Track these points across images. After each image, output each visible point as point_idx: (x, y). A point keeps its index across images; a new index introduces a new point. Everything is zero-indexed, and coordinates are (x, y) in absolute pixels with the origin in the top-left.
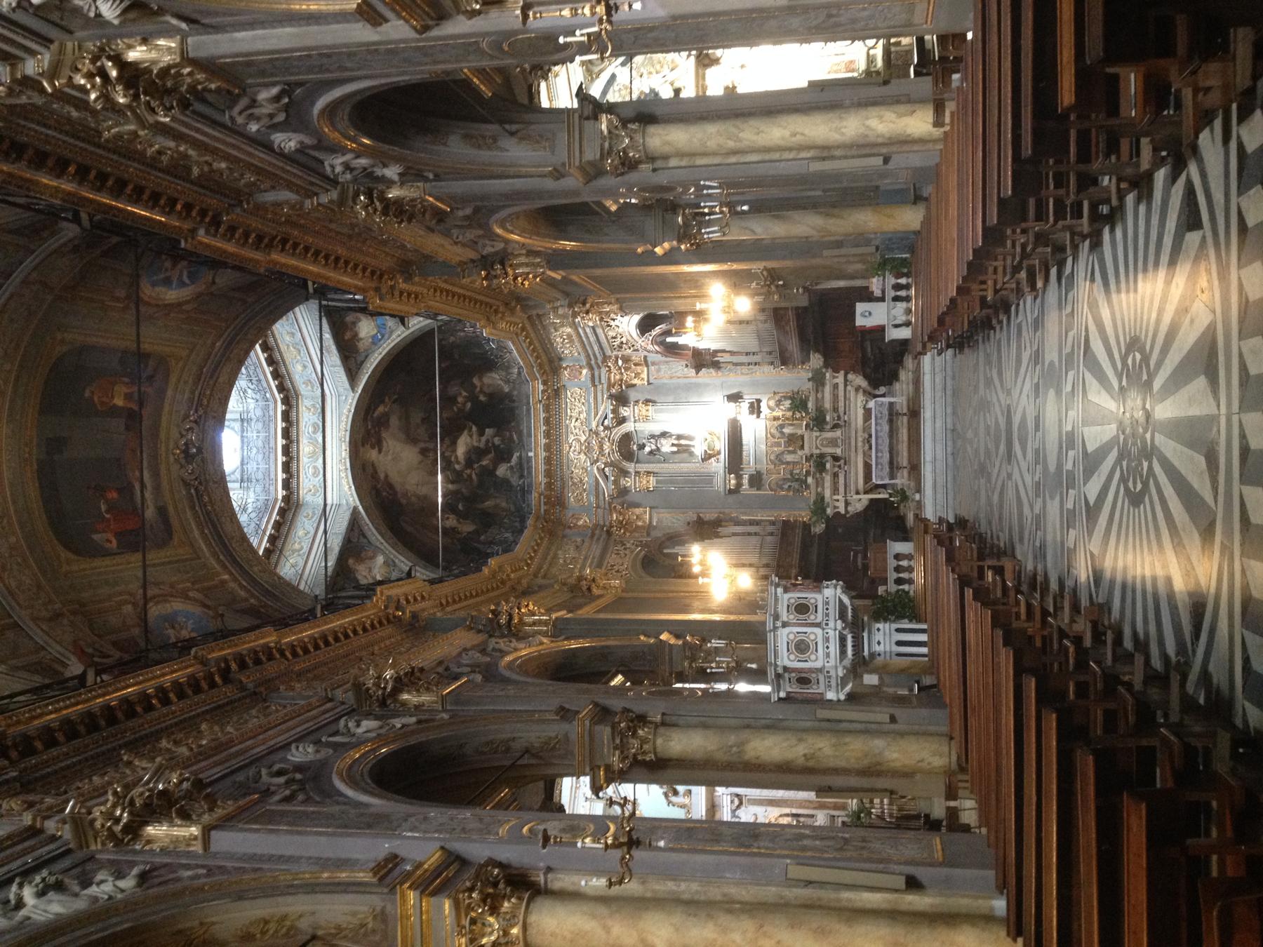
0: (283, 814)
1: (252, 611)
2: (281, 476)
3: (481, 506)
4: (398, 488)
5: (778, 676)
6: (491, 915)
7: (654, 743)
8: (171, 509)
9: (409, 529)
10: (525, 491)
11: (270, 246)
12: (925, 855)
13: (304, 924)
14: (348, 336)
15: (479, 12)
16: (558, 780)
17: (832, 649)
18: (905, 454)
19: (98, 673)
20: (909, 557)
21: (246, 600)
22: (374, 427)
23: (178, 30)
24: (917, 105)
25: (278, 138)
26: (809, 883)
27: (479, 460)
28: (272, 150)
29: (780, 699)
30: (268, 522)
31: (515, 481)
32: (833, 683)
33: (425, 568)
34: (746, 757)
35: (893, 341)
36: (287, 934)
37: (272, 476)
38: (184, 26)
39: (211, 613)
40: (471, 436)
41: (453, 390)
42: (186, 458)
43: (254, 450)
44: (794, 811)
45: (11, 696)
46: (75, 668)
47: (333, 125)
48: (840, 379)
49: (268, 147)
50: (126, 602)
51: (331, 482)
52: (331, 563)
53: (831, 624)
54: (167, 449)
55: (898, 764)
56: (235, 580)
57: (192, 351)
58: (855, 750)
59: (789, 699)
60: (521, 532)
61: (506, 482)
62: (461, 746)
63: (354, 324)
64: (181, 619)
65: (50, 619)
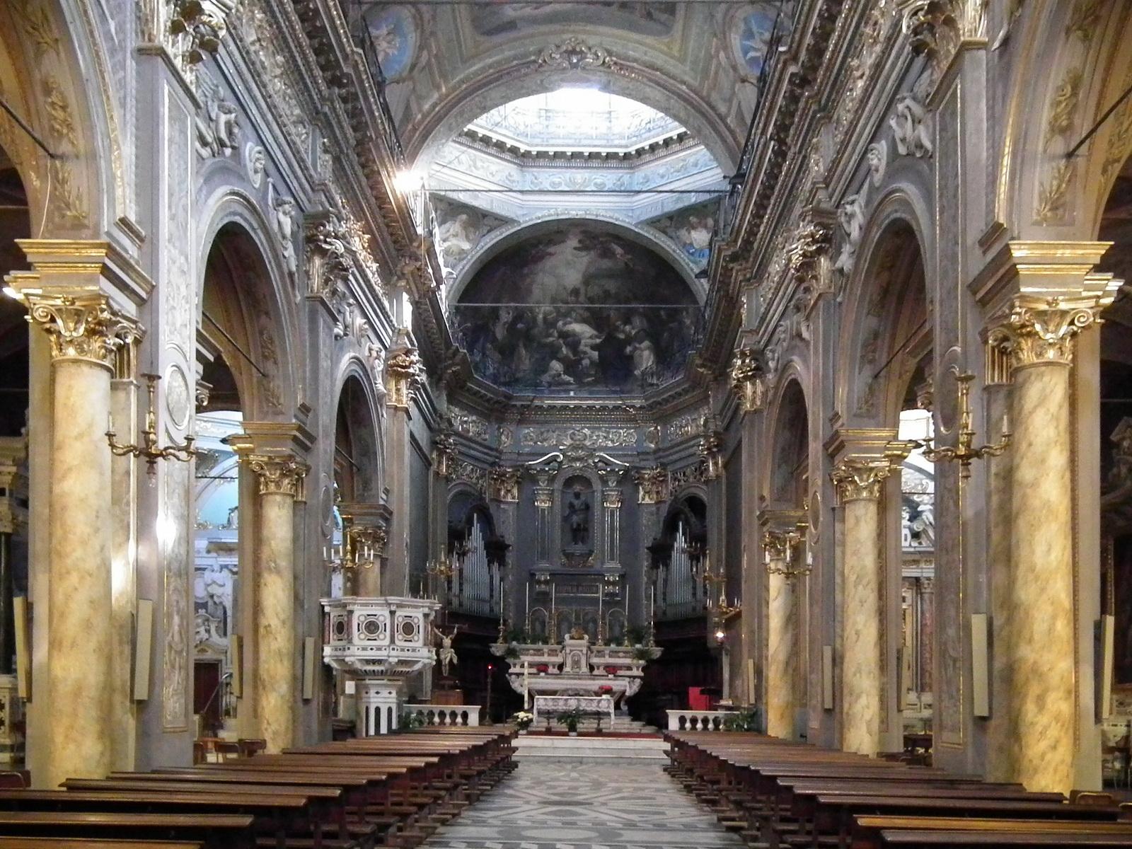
0: (183, 132)
3: (521, 345)
4: (540, 265)
5: (344, 606)
6: (86, 330)
7: (276, 493)
8: (512, 35)
12: (169, 718)
14: (693, 219)
15: (986, 342)
20: (465, 723)
21: (420, 110)
22: (601, 243)
23: (993, 40)
24: (876, 738)
27: (567, 345)
28: (871, 142)
29: (323, 607)
31: (546, 378)
35: (667, 716)
36: (52, 128)
38: (996, 45)
40: (591, 338)
41: (637, 321)
42: (566, 52)
48: (635, 672)
49: (873, 138)
52: (463, 198)
59: (323, 614)
62: (267, 314)
63: (705, 227)
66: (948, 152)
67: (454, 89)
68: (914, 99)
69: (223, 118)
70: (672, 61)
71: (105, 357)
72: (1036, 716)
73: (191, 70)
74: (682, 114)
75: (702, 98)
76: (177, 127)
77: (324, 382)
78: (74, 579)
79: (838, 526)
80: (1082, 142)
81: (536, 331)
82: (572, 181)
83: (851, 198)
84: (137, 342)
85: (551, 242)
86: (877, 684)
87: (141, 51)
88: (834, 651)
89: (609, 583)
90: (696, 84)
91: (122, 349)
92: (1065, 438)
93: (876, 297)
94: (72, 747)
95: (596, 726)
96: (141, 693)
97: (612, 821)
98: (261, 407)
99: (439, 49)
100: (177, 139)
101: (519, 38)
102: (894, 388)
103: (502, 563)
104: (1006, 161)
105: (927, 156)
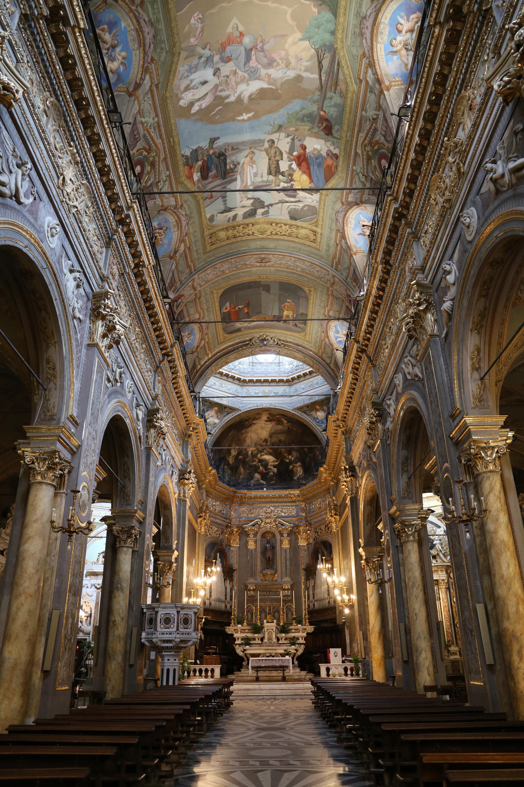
0: (101, 377)
4: (250, 429)
5: (154, 608)
8: (239, 334)
9: (231, 434)
10: (248, 487)
11: (354, 374)
13: (52, 385)
14: (317, 407)
16: (110, 501)
17: (166, 636)
18: (264, 674)
19: (169, 304)
20: (212, 677)
24: (433, 677)
25: (400, 376)
26: (50, 619)
27: (262, 465)
28: (394, 374)
29: (143, 609)
31: (252, 482)
32: (150, 636)
33: (212, 441)
34: (115, 591)
38: (443, 336)
41: (294, 453)
44: (93, 615)
45: (161, 270)
46: (172, 296)
47: (407, 400)
50: (200, 315)
51: (248, 400)
52: (216, 400)
53: (178, 636)
56: (209, 360)
57: (309, 342)
58: (117, 646)
59: (143, 614)
62: (128, 456)
63: (323, 410)
65: (193, 286)
67: (214, 355)
68: (411, 356)
69: (118, 370)
70: (306, 343)
71: (54, 480)
72: (519, 663)
74: (311, 363)
75: (319, 357)
76: (99, 375)
77: (151, 489)
78: (22, 598)
79: (400, 555)
80: (486, 374)
81: (247, 459)
84: (69, 472)
85: (255, 419)
86: (429, 644)
87: (89, 345)
88: (405, 625)
89: (284, 590)
90: (316, 351)
91: (62, 476)
92: (505, 507)
95: (282, 674)
96: (47, 667)
97: (298, 741)
100: (98, 380)
103: (231, 580)
105: (421, 380)
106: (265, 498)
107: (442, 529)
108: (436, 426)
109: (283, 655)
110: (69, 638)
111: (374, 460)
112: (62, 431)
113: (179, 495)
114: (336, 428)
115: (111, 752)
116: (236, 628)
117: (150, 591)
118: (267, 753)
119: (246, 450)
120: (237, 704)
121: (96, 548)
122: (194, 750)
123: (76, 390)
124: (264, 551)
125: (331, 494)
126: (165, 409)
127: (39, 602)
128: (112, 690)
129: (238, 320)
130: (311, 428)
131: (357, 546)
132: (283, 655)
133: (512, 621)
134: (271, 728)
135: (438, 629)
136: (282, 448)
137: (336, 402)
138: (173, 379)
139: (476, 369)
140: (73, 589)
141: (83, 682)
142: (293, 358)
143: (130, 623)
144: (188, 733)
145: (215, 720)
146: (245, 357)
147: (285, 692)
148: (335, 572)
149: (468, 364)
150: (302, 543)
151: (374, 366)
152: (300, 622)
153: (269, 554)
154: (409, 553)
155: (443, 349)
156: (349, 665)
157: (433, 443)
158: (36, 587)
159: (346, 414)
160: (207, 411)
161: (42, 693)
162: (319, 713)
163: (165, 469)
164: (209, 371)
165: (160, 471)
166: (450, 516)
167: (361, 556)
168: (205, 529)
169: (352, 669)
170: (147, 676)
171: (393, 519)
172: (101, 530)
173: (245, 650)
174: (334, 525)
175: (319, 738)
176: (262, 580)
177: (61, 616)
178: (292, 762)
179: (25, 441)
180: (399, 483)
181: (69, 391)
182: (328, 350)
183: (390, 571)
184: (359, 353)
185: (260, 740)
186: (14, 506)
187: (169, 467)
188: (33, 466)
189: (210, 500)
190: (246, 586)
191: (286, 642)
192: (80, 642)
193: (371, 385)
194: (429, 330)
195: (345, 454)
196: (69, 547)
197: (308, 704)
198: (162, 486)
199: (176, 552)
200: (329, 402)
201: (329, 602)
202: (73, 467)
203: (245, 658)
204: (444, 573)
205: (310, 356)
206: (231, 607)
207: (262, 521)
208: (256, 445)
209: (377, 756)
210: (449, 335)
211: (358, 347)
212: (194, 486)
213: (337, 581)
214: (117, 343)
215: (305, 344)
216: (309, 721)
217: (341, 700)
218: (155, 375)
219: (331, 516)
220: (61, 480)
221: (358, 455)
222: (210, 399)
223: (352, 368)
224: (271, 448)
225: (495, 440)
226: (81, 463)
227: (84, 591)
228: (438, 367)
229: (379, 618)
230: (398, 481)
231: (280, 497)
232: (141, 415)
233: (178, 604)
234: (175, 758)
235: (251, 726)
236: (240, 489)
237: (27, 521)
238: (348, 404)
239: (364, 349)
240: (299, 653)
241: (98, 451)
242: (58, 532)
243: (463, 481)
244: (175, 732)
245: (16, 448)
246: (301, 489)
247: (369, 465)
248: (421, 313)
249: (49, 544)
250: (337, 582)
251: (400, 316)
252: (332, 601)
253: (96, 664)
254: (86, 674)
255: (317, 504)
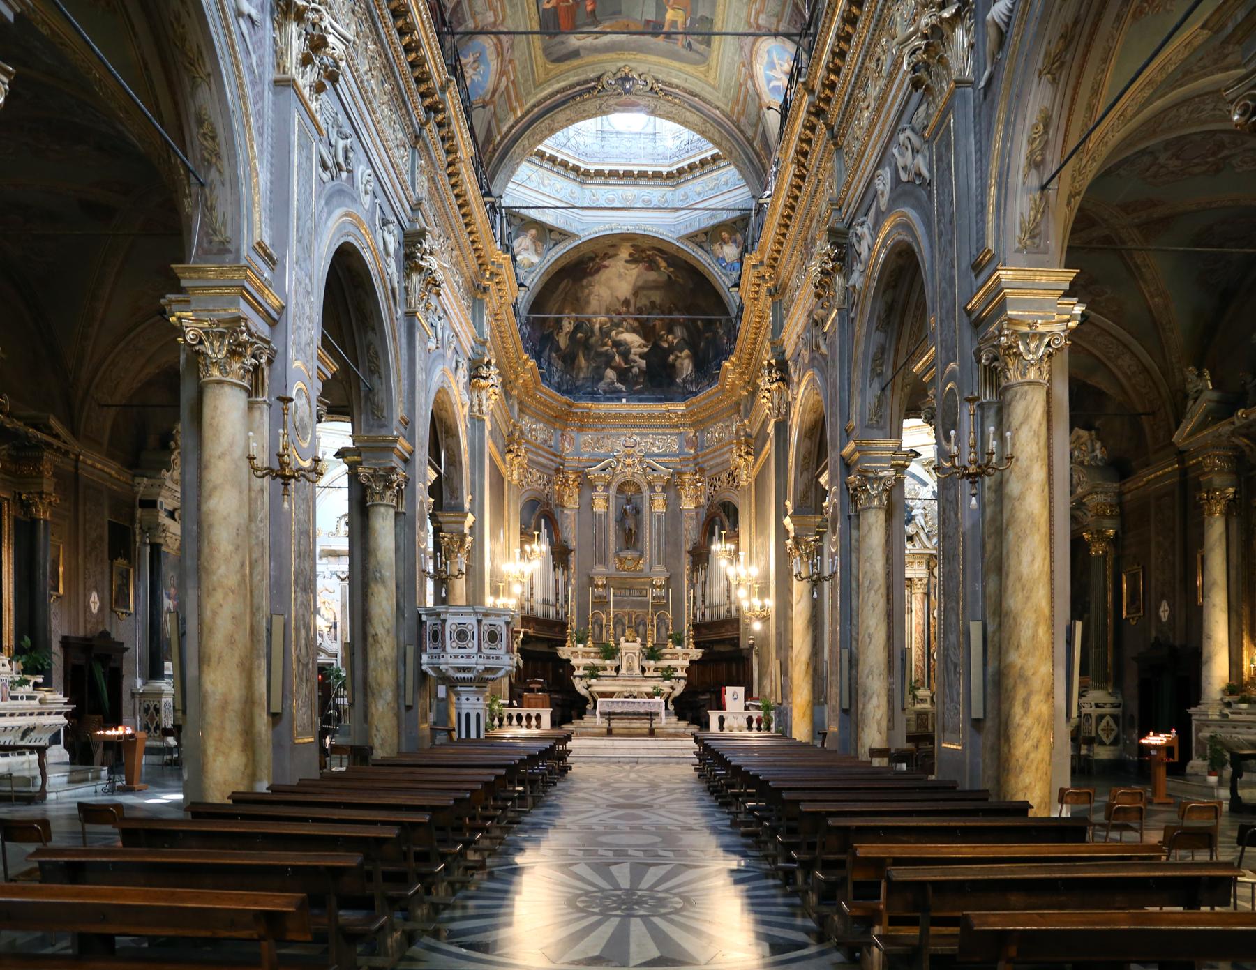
0: (309, 158)
1: (489, 137)
2: (607, 169)
4: (597, 277)
5: (438, 614)
8: (576, 62)
9: (561, 287)
10: (594, 396)
11: (800, 165)
13: (213, 174)
15: (979, 361)
16: (348, 418)
20: (538, 727)
21: (499, 133)
23: (979, 79)
25: (886, 173)
26: (269, 631)
28: (876, 169)
30: (568, 155)
31: (602, 386)
32: (435, 661)
33: (528, 301)
34: (372, 585)
36: (203, 156)
37: (607, 161)
38: (982, 84)
39: (488, 98)
41: (678, 331)
42: (621, 78)
43: (628, 145)
44: (339, 625)
49: (879, 165)
50: (496, 15)
51: (593, 215)
52: (533, 214)
53: (481, 661)
54: (630, 60)
55: (373, 710)
56: (517, 122)
57: (714, 87)
58: (384, 676)
59: (421, 623)
60: (559, 390)
61: (601, 378)
62: (373, 329)
63: (735, 242)
64: (482, 69)
66: (944, 182)
67: (528, 112)
68: (913, 130)
69: (341, 144)
70: (709, 89)
71: (243, 377)
73: (317, 99)
74: (717, 137)
75: (733, 122)
76: (304, 154)
77: (420, 396)
78: (219, 595)
79: (854, 532)
80: (1053, 177)
81: (593, 340)
82: (624, 198)
83: (862, 219)
84: (270, 361)
85: (607, 256)
86: (885, 684)
87: (277, 83)
88: (851, 653)
89: (655, 587)
90: (728, 110)
91: (257, 369)
92: (1044, 453)
93: (883, 315)
94: (221, 759)
96: (276, 708)
98: (367, 420)
99: (516, 76)
100: (304, 165)
101: (582, 66)
102: (897, 400)
104: (993, 191)
106: (624, 417)
107: (930, 488)
108: (943, 284)
109: (650, 695)
110: (304, 661)
111: (824, 349)
112: (247, 276)
113: (471, 410)
114: (757, 281)
115: (391, 833)
116: (574, 649)
117: (430, 585)
118: (624, 840)
119: (589, 320)
120: (577, 770)
121: (332, 506)
122: (515, 832)
123: (262, 187)
124: (622, 517)
125: (742, 414)
126: (437, 231)
127: (248, 602)
128: (382, 745)
129: (574, 30)
130: (711, 279)
131: (781, 512)
132: (650, 695)
133: (1023, 652)
134: (630, 805)
135: (903, 660)
136: (656, 319)
137: (761, 226)
138: (450, 164)
139: (1036, 164)
140: (301, 580)
141: (335, 731)
142: (682, 124)
143: (402, 638)
144: (504, 809)
145: (544, 792)
146: (589, 117)
147: (653, 753)
148: (742, 558)
149: (1022, 152)
150: (688, 504)
151: (839, 148)
152: (679, 642)
153: (630, 523)
154: (870, 529)
155: (977, 115)
156: (755, 714)
157: (933, 321)
158: (239, 576)
159: (778, 252)
160: (517, 237)
161: (274, 747)
162: (705, 785)
163: (444, 356)
164: (517, 149)
165: (434, 361)
166: (947, 465)
167: (787, 531)
168: (519, 475)
169: (759, 721)
170: (435, 723)
171: (847, 466)
172: (337, 473)
173: (589, 686)
174: (743, 474)
175: (703, 821)
176: (617, 569)
177: (286, 625)
178: (661, 853)
179: (181, 297)
180: (864, 398)
181: (249, 189)
182: (752, 109)
183: (833, 561)
184: (812, 118)
185: (612, 821)
186: (179, 427)
187: (450, 353)
188: (201, 348)
189: (527, 419)
190: (591, 579)
191: (655, 674)
192: (322, 669)
193: (829, 190)
194: (956, 67)
195: (770, 336)
196: (286, 505)
197: (688, 771)
198: (439, 391)
199: (470, 515)
200: (747, 225)
201: (728, 611)
202: (275, 352)
203: (591, 700)
204: (924, 566)
205: (715, 121)
206: (566, 614)
207: (618, 462)
208: (608, 312)
209: (788, 847)
210: (995, 83)
211: (811, 104)
212: (497, 390)
213: (746, 575)
214: (333, 78)
215: (707, 92)
216: (688, 796)
217: (740, 767)
218: (413, 153)
219: (740, 456)
220: (257, 377)
221: (794, 338)
222: (522, 211)
223: (796, 151)
224: (636, 319)
225: (1048, 320)
226: (290, 344)
227: (320, 583)
228: (962, 157)
229: (809, 639)
230: (863, 391)
231: (651, 416)
232: (392, 245)
233: (478, 608)
234: (486, 843)
235: (599, 802)
236: (580, 399)
237: (206, 456)
238: (783, 230)
239: (822, 107)
240: (677, 693)
241: (318, 319)
242: (263, 477)
243: (978, 398)
244: (485, 808)
245: (164, 312)
246: (688, 402)
247: (812, 359)
248: (945, 27)
249: (250, 499)
250: (743, 577)
251: (901, 31)
252: (733, 608)
253: (352, 705)
254: (339, 719)
255: (716, 432)
